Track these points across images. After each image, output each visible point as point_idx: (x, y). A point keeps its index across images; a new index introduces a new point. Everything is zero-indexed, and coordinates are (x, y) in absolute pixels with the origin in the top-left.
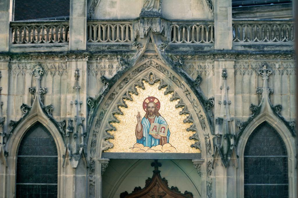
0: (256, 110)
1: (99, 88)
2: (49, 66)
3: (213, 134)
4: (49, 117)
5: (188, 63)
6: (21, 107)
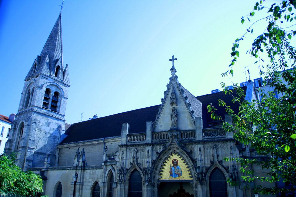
0: (212, 163)
1: (156, 156)
2: (139, 149)
3: (196, 172)
4: (139, 167)
5: (187, 146)
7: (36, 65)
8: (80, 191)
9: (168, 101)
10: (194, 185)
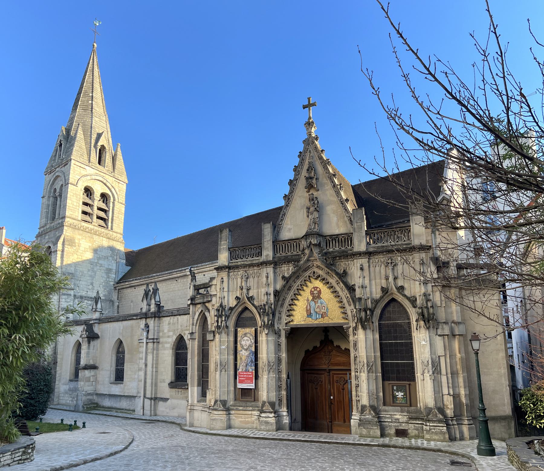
0: (385, 291)
7: (61, 145)
8: (155, 352)
9: (302, 183)
10: (351, 329)
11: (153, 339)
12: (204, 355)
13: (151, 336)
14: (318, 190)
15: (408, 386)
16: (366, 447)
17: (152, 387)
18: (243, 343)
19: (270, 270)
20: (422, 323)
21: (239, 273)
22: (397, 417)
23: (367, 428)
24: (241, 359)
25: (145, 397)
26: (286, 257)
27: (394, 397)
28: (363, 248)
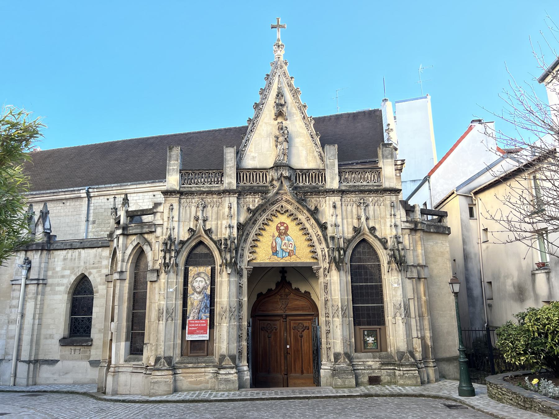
0: (357, 230)
6: (188, 230)
8: (39, 297)
10: (322, 270)
11: (38, 280)
12: (138, 301)
13: (33, 275)
14: (287, 120)
15: (378, 330)
16: (349, 399)
17: (31, 346)
18: (196, 284)
19: (233, 200)
20: (394, 265)
21: (193, 201)
22: (370, 363)
23: (342, 378)
24: (192, 304)
25: (18, 359)
26: (252, 187)
27: (365, 342)
28: (335, 185)
